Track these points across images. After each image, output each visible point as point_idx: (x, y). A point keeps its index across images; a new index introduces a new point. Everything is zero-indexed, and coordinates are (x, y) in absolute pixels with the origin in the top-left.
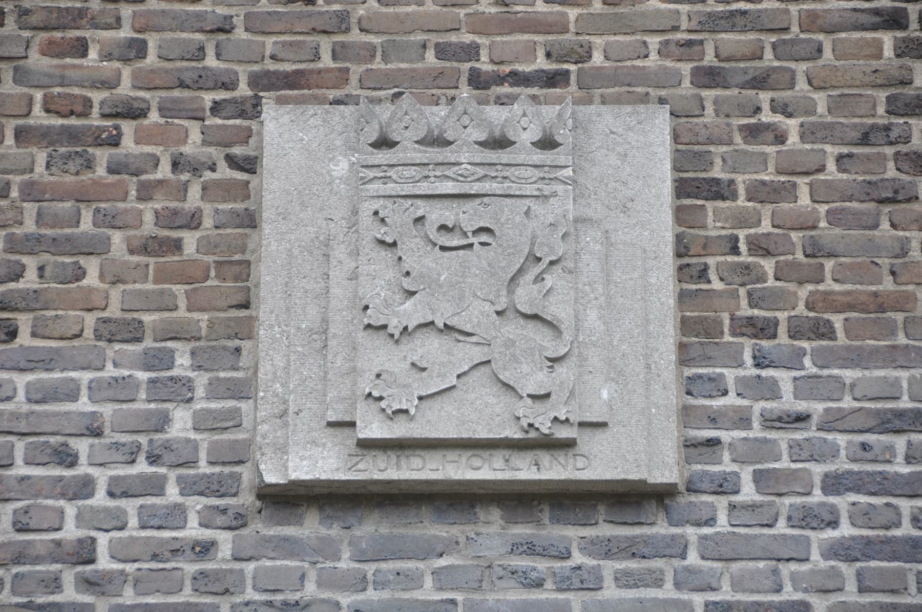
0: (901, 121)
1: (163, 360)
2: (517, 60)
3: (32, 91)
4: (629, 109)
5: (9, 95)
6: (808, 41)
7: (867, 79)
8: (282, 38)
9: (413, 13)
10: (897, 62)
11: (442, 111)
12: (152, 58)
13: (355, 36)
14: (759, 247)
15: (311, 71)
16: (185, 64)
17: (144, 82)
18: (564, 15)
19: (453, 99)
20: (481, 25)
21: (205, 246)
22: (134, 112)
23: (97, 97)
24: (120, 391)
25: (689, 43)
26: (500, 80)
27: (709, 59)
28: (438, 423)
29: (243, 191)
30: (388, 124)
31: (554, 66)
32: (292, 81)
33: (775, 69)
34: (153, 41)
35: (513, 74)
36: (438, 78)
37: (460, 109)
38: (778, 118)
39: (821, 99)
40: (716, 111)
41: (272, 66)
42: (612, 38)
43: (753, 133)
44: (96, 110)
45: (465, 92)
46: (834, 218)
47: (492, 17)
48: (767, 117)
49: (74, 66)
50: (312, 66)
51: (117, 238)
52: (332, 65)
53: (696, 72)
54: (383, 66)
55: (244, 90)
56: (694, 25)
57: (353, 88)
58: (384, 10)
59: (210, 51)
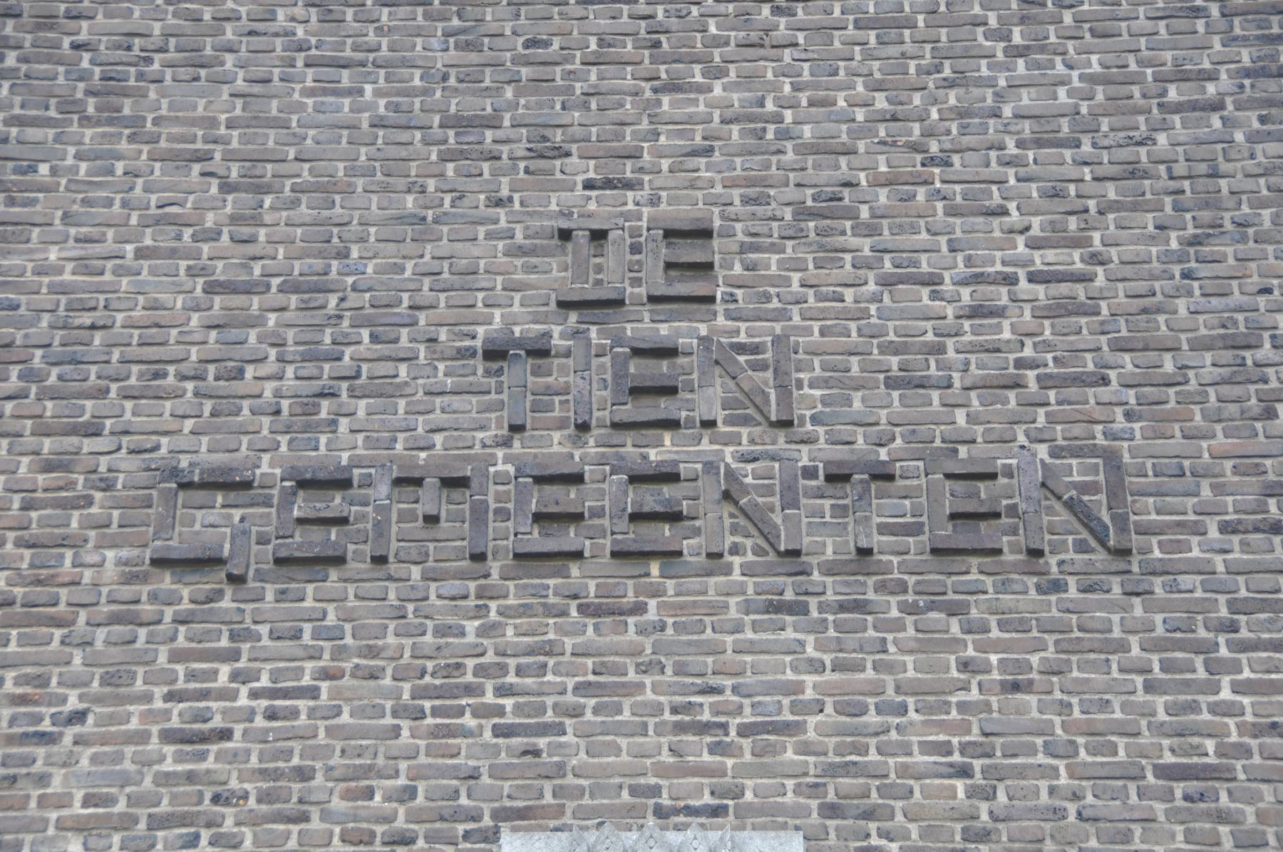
0: (973, 846)
2: (689, 797)
3: (332, 827)
4: (773, 834)
5: (316, 831)
6: (904, 785)
7: (946, 815)
8: (516, 782)
9: (613, 763)
10: (968, 802)
11: (634, 835)
12: (420, 799)
13: (570, 780)
15: (537, 807)
16: (445, 803)
18: (724, 764)
19: (642, 826)
20: (662, 771)
23: (379, 829)
25: (816, 785)
26: (677, 811)
27: (831, 797)
30: (594, 846)
31: (717, 802)
32: (522, 814)
33: (879, 805)
34: (421, 787)
35: (687, 807)
36: (630, 811)
37: (647, 834)
38: (883, 842)
39: (914, 829)
40: (837, 836)
41: (508, 803)
42: (759, 781)
44: (378, 839)
45: (651, 821)
47: (671, 765)
49: (364, 807)
50: (538, 802)
52: (553, 802)
53: (821, 806)
54: (590, 802)
55: (487, 821)
56: (819, 771)
57: (568, 819)
58: (591, 760)
59: (463, 793)
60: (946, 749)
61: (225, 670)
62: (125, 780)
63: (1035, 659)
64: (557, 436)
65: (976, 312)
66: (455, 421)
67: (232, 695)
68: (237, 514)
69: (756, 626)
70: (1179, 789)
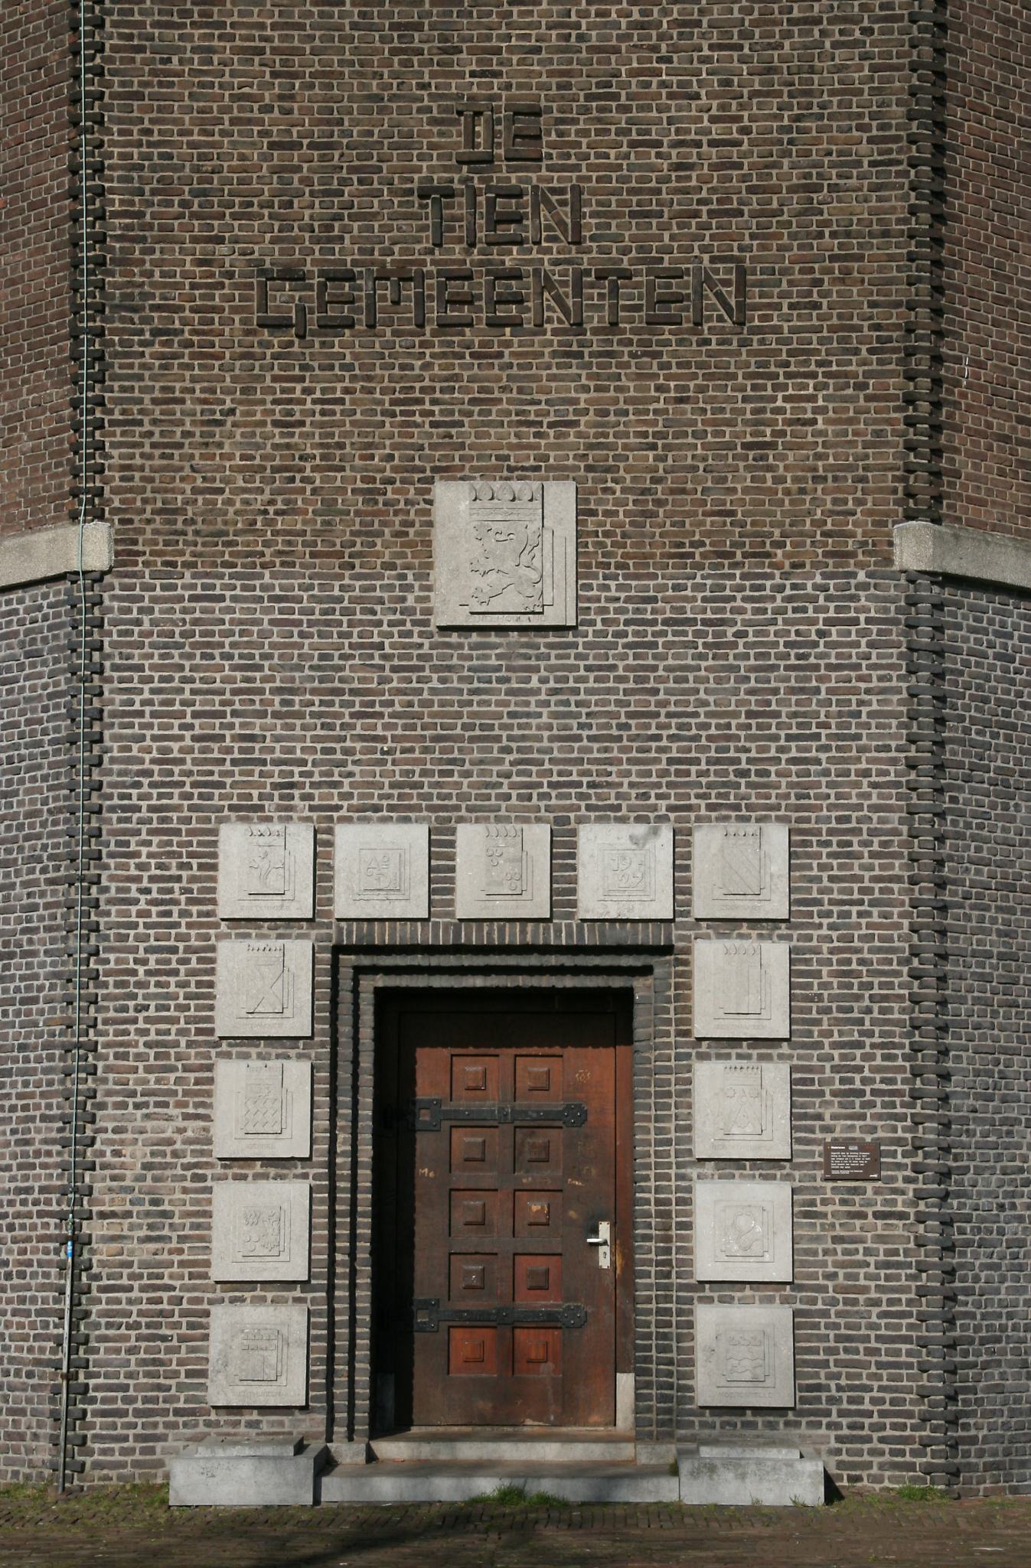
1: (404, 577)
13: (467, 452)
14: (606, 534)
17: (394, 469)
20: (511, 447)
21: (417, 534)
22: (391, 481)
24: (390, 588)
27: (590, 462)
28: (496, 605)
29: (428, 513)
43: (605, 490)
46: (631, 523)
48: (610, 484)
51: (387, 531)
60: (645, 435)
61: (299, 387)
62: (258, 447)
63: (692, 384)
64: (457, 248)
65: (678, 167)
66: (407, 239)
67: (303, 402)
68: (297, 295)
69: (559, 366)
70: (751, 454)
